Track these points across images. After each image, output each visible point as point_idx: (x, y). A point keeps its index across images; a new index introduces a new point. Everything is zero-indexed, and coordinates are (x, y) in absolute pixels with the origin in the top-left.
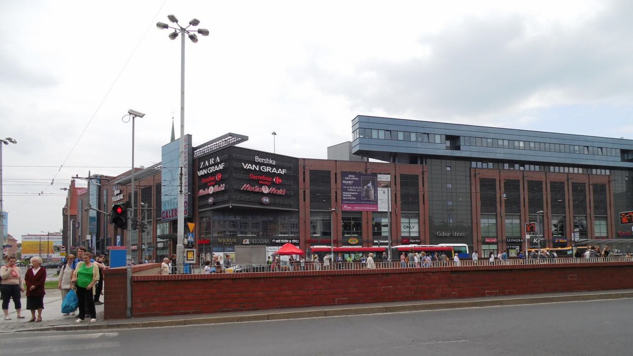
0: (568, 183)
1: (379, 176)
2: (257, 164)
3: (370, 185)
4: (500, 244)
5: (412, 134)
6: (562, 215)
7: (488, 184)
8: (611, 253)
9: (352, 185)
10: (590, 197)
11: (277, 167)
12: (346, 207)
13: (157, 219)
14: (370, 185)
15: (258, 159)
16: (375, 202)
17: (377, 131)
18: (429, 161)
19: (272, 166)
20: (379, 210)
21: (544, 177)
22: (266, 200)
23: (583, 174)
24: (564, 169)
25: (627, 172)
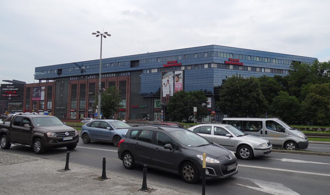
0: (107, 82)
1: (42, 87)
2: (7, 88)
3: (39, 91)
4: (85, 112)
5: (257, 68)
7: (74, 87)
9: (36, 91)
10: (78, 90)
11: (15, 88)
12: (33, 99)
13: (80, 99)
14: (39, 91)
15: (8, 87)
16: (40, 97)
17: (264, 69)
19: (13, 88)
20: (41, 100)
21: (96, 80)
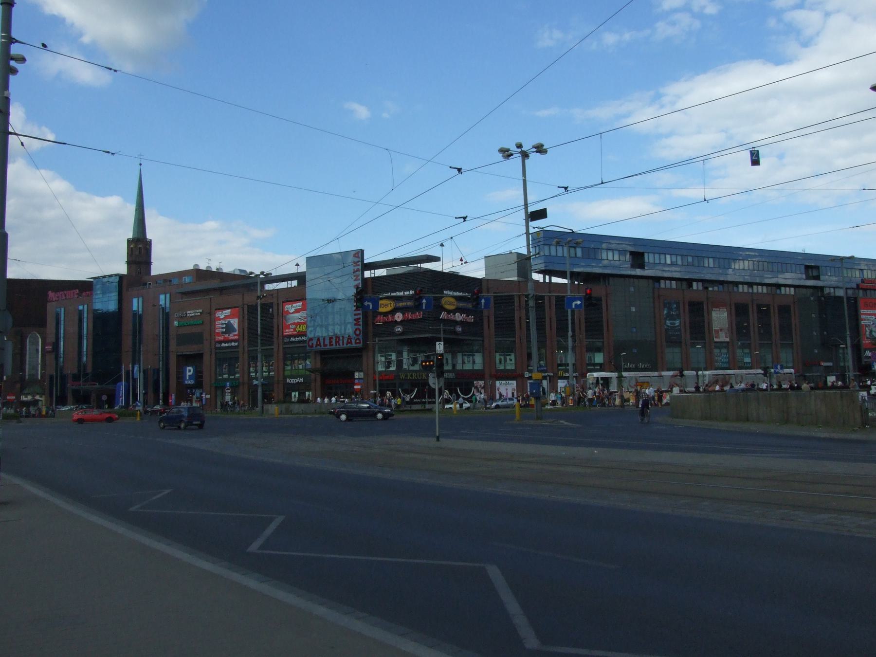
6: (702, 341)
8: (766, 378)
10: (775, 321)
13: (284, 346)
18: (611, 279)
22: (459, 329)
23: (677, 289)
24: (743, 287)
25: (811, 290)
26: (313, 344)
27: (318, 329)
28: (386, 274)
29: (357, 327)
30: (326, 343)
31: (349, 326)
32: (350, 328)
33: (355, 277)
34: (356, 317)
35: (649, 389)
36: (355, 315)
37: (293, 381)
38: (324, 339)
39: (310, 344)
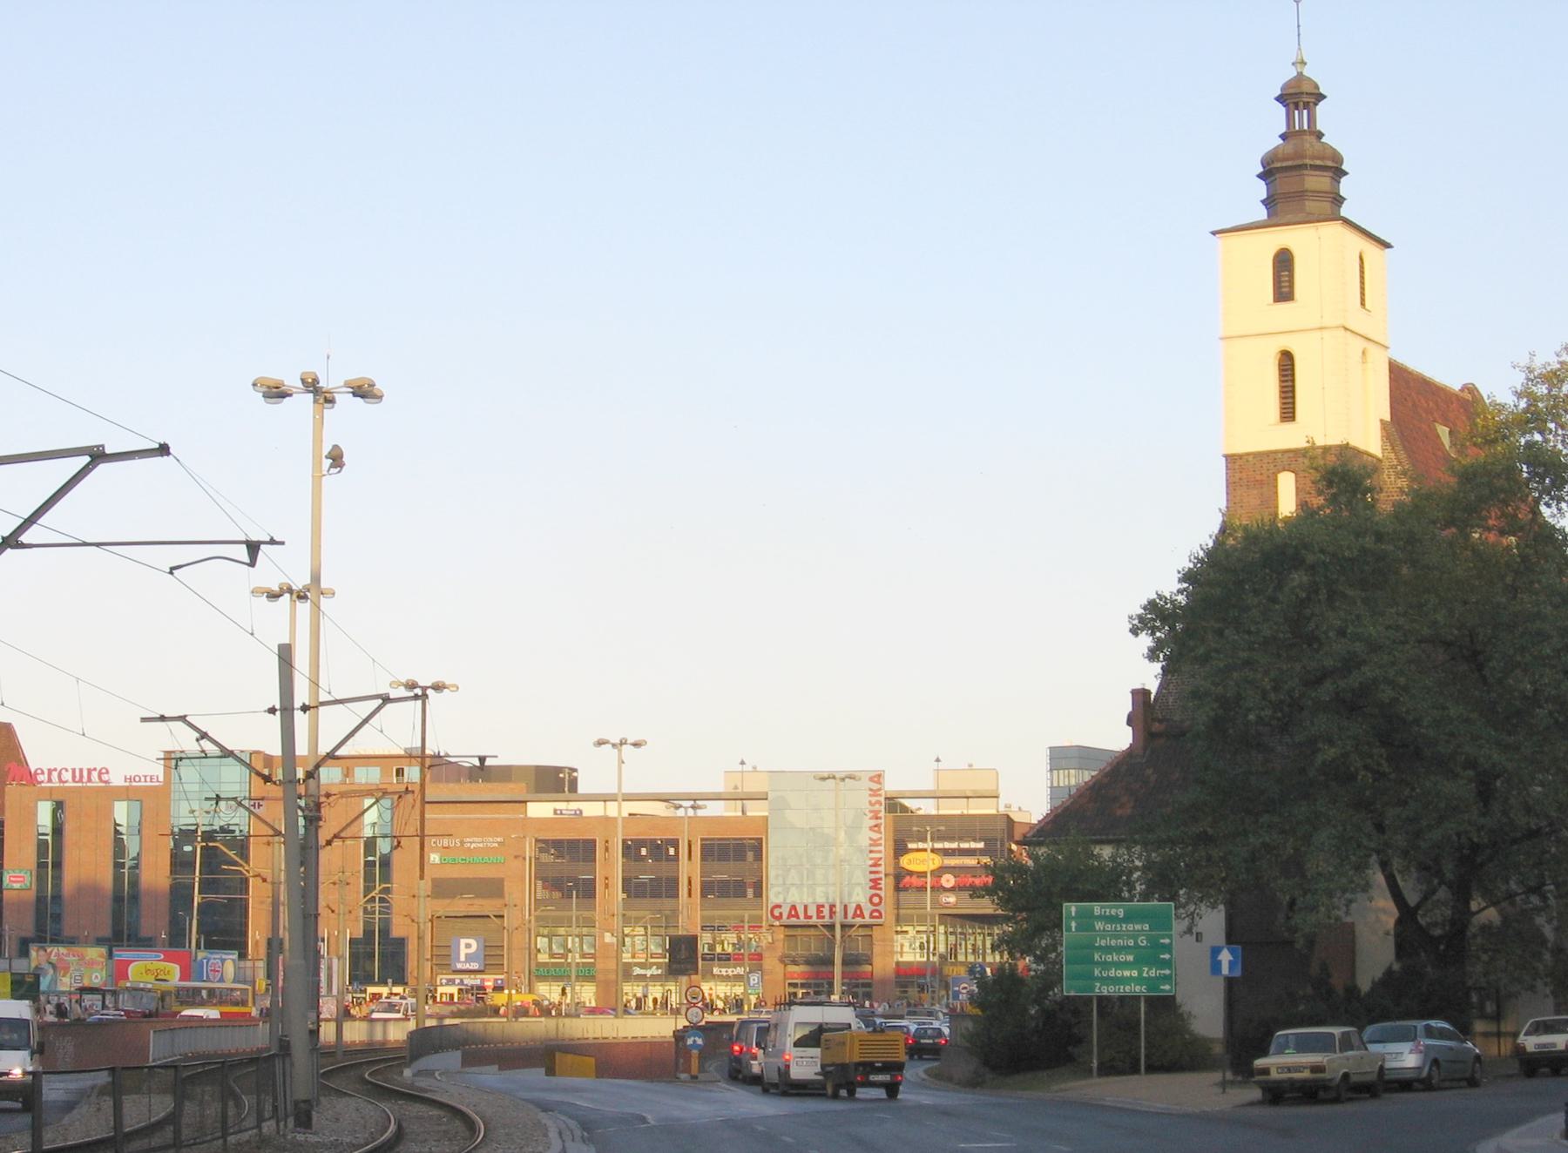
26: (781, 914)
27: (793, 890)
28: (297, 753)
29: (874, 892)
30: (809, 914)
31: (858, 890)
32: (860, 892)
33: (872, 814)
34: (873, 876)
35: (974, 1008)
36: (871, 872)
37: (727, 972)
38: (806, 907)
39: (776, 913)
